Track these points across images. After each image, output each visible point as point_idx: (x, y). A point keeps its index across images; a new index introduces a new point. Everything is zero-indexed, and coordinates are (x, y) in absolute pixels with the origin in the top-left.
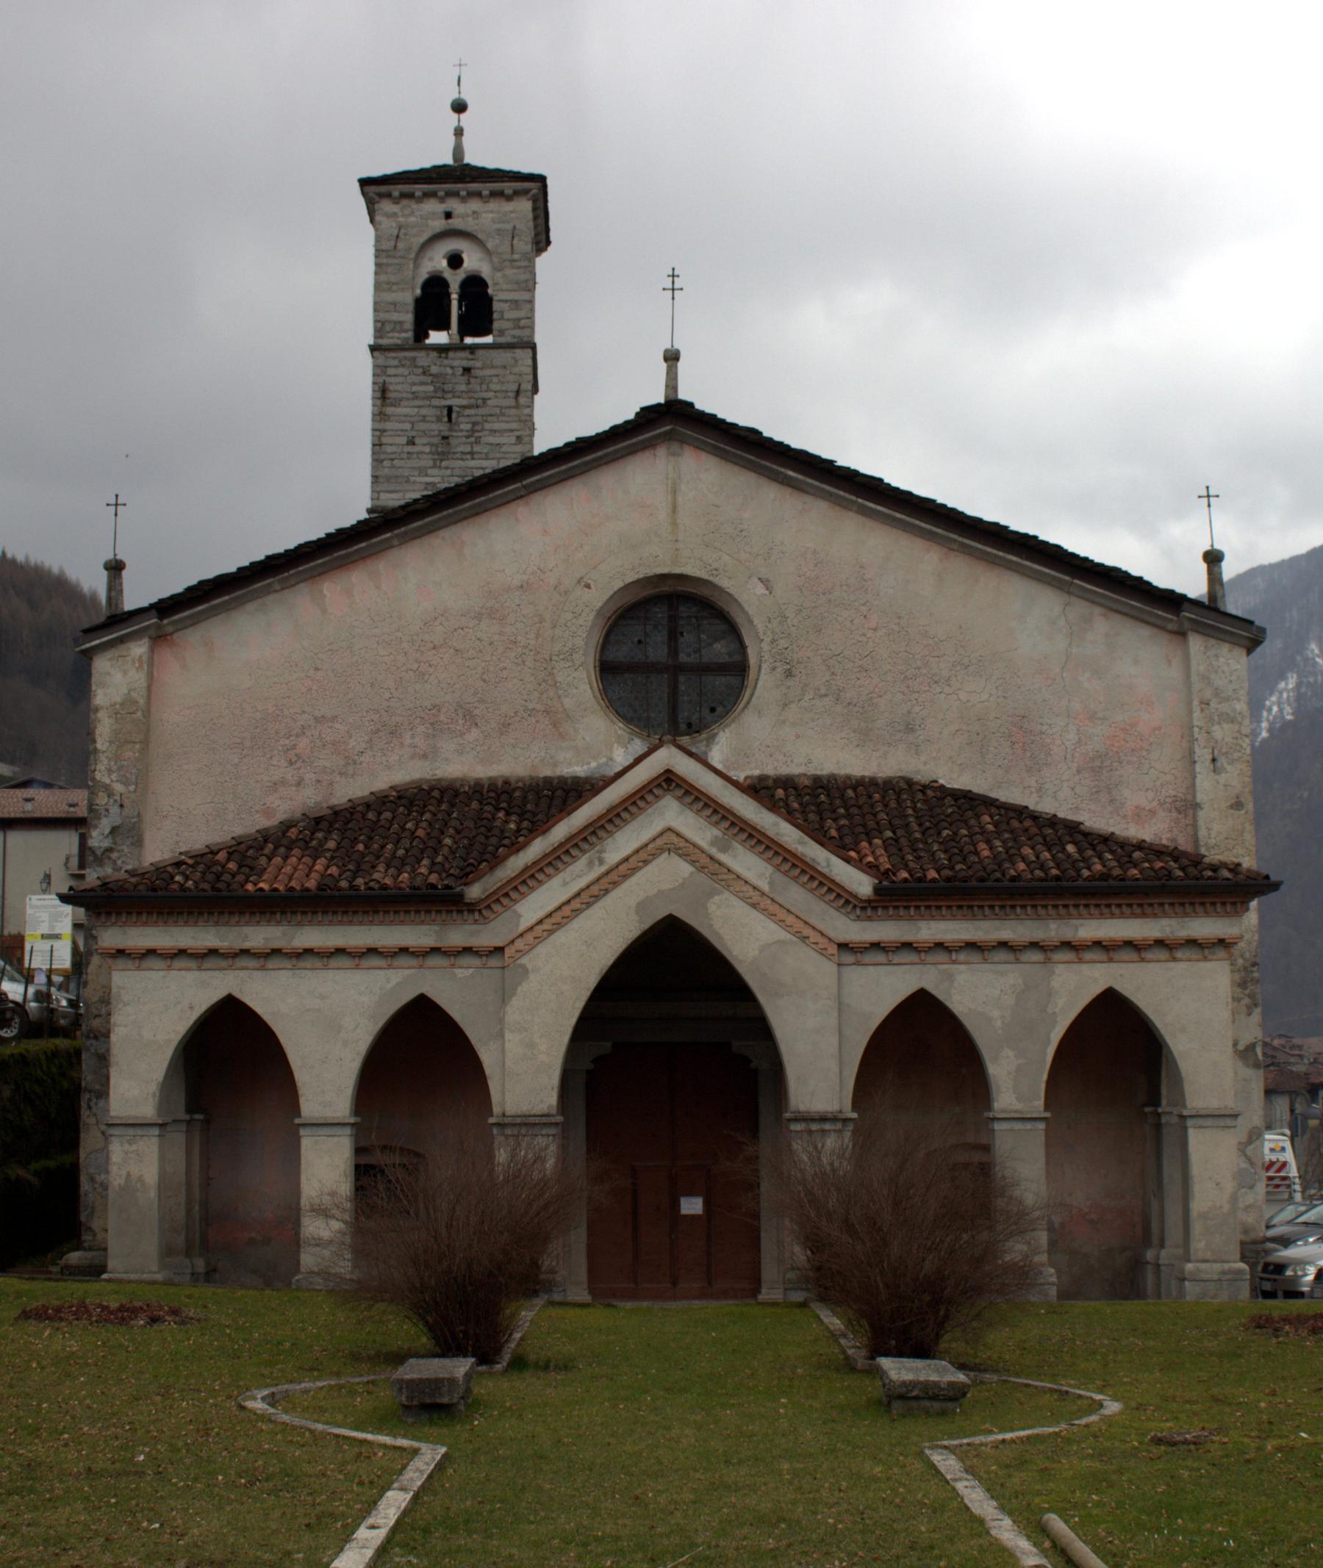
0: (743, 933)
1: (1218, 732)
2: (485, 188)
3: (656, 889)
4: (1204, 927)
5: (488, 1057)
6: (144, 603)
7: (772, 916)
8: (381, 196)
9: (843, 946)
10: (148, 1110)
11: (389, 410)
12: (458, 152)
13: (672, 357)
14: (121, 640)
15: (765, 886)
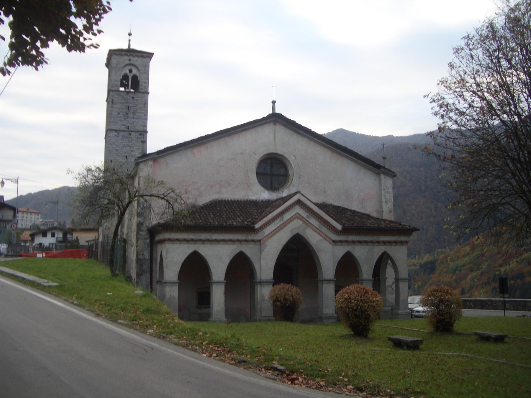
0: (313, 238)
1: (387, 196)
2: (134, 54)
3: (295, 227)
4: (403, 238)
5: (257, 266)
6: (154, 151)
7: (319, 234)
8: (114, 54)
9: (334, 241)
10: (175, 279)
11: (114, 106)
12: (129, 46)
13: (274, 102)
14: (147, 160)
15: (317, 227)
